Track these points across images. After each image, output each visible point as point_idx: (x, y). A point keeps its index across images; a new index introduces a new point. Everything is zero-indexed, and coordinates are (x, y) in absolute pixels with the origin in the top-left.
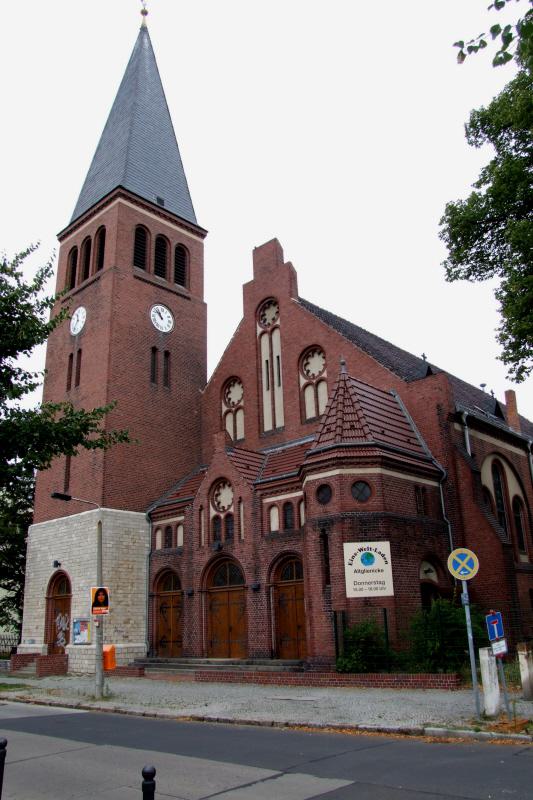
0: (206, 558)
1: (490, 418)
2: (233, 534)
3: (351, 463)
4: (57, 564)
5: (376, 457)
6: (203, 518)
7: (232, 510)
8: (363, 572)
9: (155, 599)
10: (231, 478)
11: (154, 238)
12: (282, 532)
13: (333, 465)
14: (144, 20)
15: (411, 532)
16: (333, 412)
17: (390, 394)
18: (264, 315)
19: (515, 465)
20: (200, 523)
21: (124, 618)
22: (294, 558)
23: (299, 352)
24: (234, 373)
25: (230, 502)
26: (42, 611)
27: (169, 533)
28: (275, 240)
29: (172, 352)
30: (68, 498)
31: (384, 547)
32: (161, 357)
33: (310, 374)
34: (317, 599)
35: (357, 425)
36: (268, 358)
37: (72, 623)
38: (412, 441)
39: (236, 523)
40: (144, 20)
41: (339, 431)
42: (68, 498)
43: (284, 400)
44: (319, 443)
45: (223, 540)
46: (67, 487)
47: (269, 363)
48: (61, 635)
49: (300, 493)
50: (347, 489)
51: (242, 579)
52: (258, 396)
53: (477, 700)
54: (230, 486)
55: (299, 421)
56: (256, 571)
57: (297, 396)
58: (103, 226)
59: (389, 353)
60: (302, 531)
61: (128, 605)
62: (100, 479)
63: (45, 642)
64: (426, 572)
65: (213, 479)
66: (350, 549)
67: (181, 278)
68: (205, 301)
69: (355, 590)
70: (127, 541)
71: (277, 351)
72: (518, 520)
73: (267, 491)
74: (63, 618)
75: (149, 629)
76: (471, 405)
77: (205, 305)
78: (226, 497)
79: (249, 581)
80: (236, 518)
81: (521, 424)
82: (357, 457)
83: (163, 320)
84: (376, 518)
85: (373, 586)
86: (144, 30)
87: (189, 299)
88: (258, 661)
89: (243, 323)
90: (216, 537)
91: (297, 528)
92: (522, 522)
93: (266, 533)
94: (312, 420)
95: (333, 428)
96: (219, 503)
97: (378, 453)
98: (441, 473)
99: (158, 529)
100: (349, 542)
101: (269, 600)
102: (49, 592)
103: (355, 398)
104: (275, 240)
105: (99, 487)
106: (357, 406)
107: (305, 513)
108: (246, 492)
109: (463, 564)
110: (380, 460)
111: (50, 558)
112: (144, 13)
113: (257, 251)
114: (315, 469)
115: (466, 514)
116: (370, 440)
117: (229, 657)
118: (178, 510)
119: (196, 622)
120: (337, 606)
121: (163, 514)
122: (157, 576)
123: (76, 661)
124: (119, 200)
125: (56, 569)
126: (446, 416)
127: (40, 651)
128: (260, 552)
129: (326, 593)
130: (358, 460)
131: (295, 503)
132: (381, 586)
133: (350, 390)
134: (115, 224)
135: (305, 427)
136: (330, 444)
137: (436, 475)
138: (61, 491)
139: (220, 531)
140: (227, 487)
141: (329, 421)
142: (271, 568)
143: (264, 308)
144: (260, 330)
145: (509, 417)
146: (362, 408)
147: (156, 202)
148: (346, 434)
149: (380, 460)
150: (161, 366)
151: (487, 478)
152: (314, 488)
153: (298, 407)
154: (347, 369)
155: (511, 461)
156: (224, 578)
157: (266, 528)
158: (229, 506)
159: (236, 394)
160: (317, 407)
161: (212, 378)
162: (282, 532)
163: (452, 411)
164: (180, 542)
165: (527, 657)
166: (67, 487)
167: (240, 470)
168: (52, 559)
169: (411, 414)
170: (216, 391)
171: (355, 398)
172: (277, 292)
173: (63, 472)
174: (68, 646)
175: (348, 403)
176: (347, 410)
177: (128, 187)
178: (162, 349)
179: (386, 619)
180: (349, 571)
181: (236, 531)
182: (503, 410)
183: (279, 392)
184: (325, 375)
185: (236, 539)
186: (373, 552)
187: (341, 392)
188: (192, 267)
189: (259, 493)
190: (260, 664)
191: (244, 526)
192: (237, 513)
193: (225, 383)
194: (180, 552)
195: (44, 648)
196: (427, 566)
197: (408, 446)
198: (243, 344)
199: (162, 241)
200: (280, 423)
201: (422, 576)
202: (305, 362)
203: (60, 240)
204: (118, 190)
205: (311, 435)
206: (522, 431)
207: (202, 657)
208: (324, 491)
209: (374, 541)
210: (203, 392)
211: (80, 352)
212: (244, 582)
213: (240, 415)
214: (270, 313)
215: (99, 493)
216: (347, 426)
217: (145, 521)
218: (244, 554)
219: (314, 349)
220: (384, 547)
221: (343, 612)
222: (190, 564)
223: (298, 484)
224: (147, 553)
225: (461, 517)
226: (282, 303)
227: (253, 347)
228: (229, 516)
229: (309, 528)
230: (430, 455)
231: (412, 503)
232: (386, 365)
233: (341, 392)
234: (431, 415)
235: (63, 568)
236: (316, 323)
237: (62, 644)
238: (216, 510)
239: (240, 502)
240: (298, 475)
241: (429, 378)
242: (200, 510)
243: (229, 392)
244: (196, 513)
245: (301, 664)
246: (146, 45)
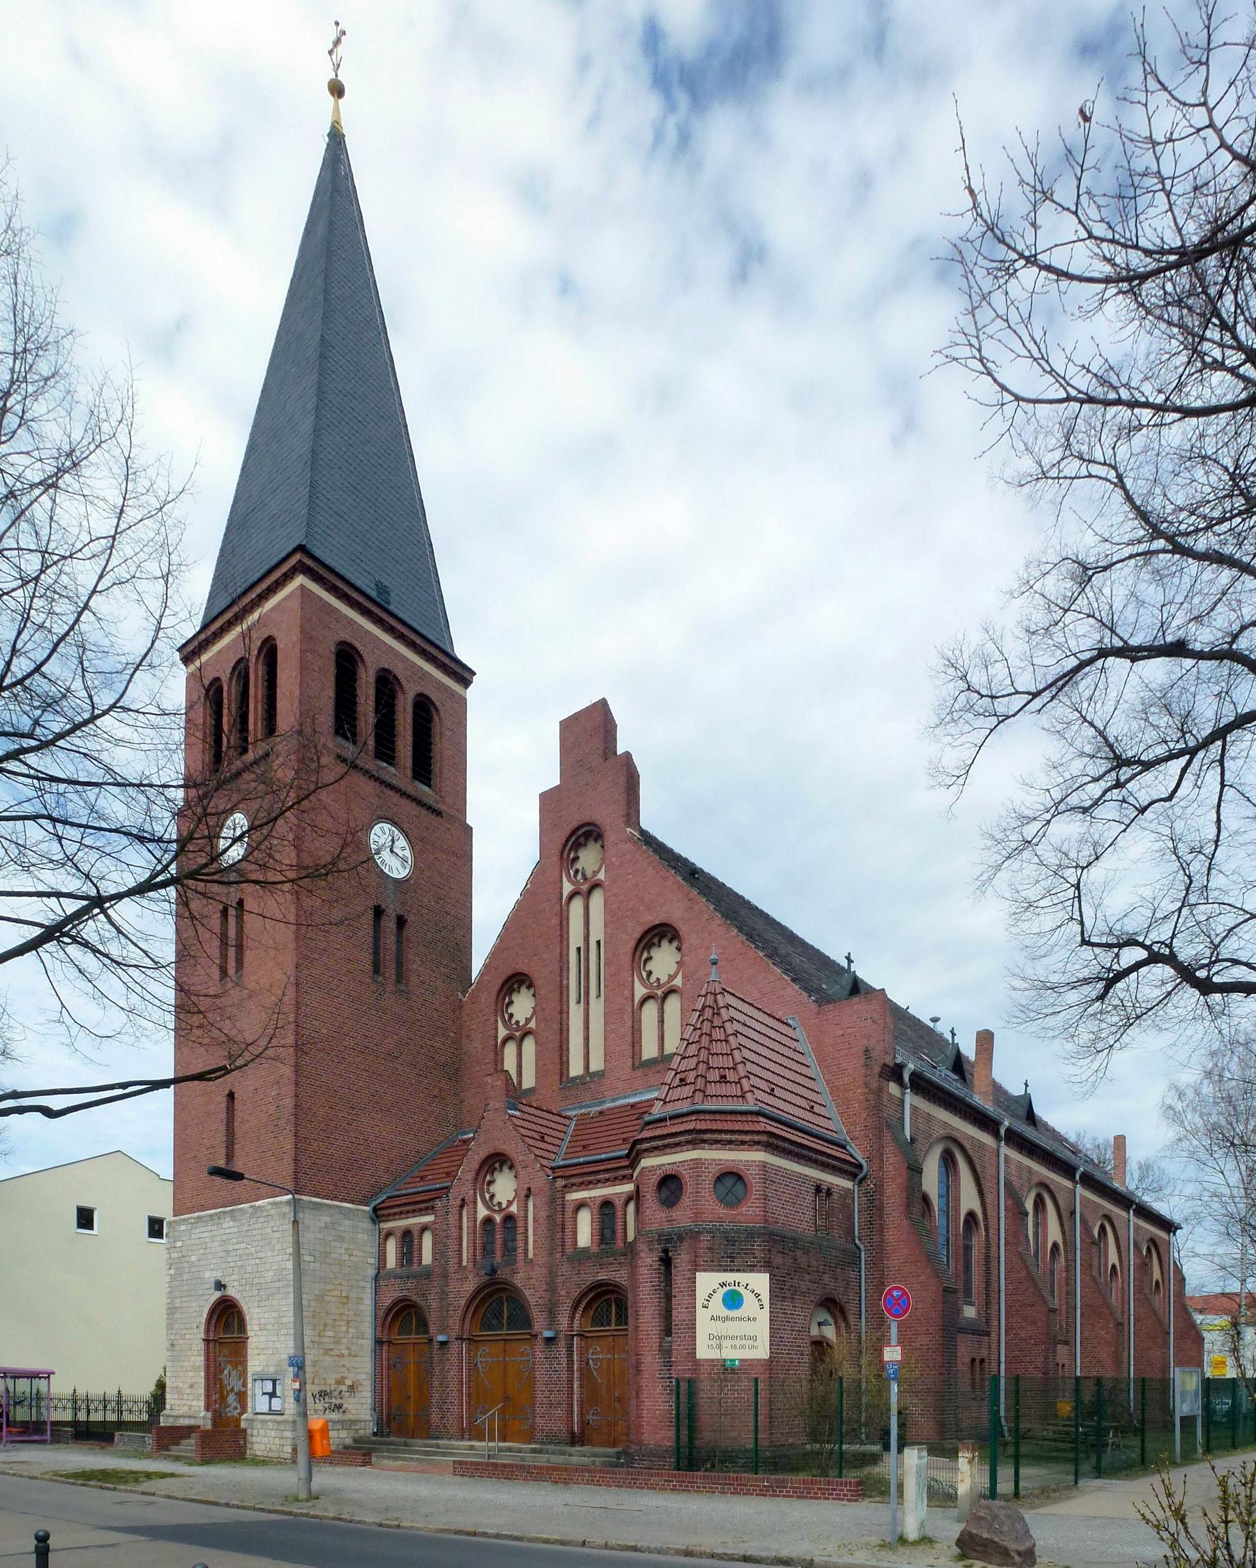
0: (470, 1286)
1: (943, 1076)
2: (515, 1249)
3: (717, 1142)
4: (220, 1286)
5: (758, 1133)
6: (465, 1220)
7: (514, 1209)
8: (727, 1319)
9: (385, 1347)
10: (513, 1155)
11: (371, 678)
12: (595, 1249)
13: (688, 1142)
14: (337, 109)
15: (803, 1261)
16: (693, 1050)
17: (790, 1026)
18: (576, 859)
19: (976, 1161)
20: (461, 1228)
22: (613, 1292)
23: (637, 935)
24: (521, 968)
25: (511, 1196)
26: (200, 1360)
27: (408, 1240)
28: (603, 703)
29: (411, 918)
30: (238, 1177)
31: (760, 1282)
32: (389, 924)
33: (653, 979)
35: (731, 1076)
36: (581, 944)
37: (250, 1380)
38: (817, 1109)
39: (520, 1230)
40: (337, 109)
41: (700, 1083)
42: (238, 1177)
43: (606, 1023)
44: (665, 1103)
45: (498, 1259)
46: (230, 1156)
47: (584, 953)
48: (231, 1399)
49: (629, 1187)
50: (707, 1184)
51: (527, 1322)
52: (561, 1013)
53: (894, 1517)
54: (511, 1168)
55: (630, 1063)
56: (552, 1314)
57: (627, 1017)
59: (790, 950)
60: (631, 1251)
61: (343, 1356)
62: (289, 1145)
63: (207, 1408)
64: (820, 1324)
65: (483, 1153)
66: (707, 1282)
67: (423, 768)
71: (597, 932)
72: (967, 1249)
73: (573, 1180)
74: (234, 1373)
75: (376, 1392)
76: (915, 1051)
77: (469, 830)
78: (504, 1187)
80: (520, 1223)
81: (995, 1095)
82: (727, 1132)
84: (751, 1234)
85: (738, 1342)
86: (336, 140)
87: (439, 813)
88: (551, 1447)
89: (539, 873)
90: (487, 1250)
91: (620, 1244)
92: (975, 1252)
93: (569, 1250)
94: (653, 1062)
95: (691, 1079)
96: (492, 1196)
97: (764, 1125)
98: (860, 1166)
99: (389, 1234)
100: (705, 1270)
101: (570, 1355)
102: (207, 1331)
103: (730, 1028)
104: (603, 703)
105: (289, 1158)
106: (733, 1041)
107: (637, 1220)
108: (539, 1180)
110: (764, 1138)
111: (207, 1275)
112: (337, 90)
114: (656, 1148)
115: (891, 1236)
116: (750, 1106)
118: (423, 1203)
119: (453, 1385)
120: (681, 1370)
121: (397, 1210)
122: (389, 1310)
123: (259, 1439)
124: (300, 580)
125: (218, 1294)
126: (877, 1070)
128: (560, 1280)
129: (666, 1352)
130: (728, 1137)
131: (619, 1204)
132: (751, 1342)
133: (723, 1011)
134: (295, 637)
135: (638, 1073)
136: (684, 1107)
137: (852, 1170)
138: (221, 1163)
139: (493, 1243)
140: (505, 1169)
141: (686, 1064)
142: (575, 1308)
143: (577, 846)
144: (568, 888)
145: (978, 1080)
146: (740, 1047)
147: (374, 594)
148: (712, 1089)
149: (764, 1138)
151: (931, 1181)
152: (654, 1180)
153: (629, 1038)
154: (719, 973)
155: (970, 1151)
156: (498, 1315)
157: (569, 1242)
158: (510, 1203)
159: (522, 1006)
160: (520, 1055)
161: (482, 974)
162: (595, 1249)
163: (889, 1060)
164: (427, 1257)
165: (970, 1462)
166: (230, 1156)
167: (531, 1142)
168: (210, 1276)
169: (821, 1061)
170: (488, 998)
171: (730, 1028)
172: (607, 816)
173: (223, 1128)
174: (244, 1416)
175: (718, 1035)
176: (716, 1048)
177: (318, 553)
178: (391, 911)
179: (757, 1393)
180: (702, 1316)
181: (520, 1244)
182: (966, 1066)
183: (597, 1008)
184: (678, 982)
185: (520, 1257)
186: (741, 1290)
187: (708, 1013)
188: (441, 747)
189: (560, 1183)
190: (553, 1453)
191: (532, 1239)
192: (522, 1213)
194: (427, 1274)
196: (823, 1315)
197: (809, 1116)
199: (387, 684)
200: (597, 1064)
201: (815, 1331)
202: (645, 955)
203: (186, 660)
204: (298, 557)
205: (650, 1088)
206: (998, 1103)
207: (462, 1439)
208: (670, 1184)
212: (530, 1326)
213: (529, 1045)
214: (589, 858)
215: (287, 1169)
216: (714, 1075)
218: (533, 1281)
219: (660, 933)
220: (760, 1282)
221: (690, 1381)
222: (443, 1295)
223: (626, 1172)
224: (371, 1272)
225: (882, 1241)
226: (610, 836)
227: (555, 921)
228: (509, 1218)
229: (642, 1247)
230: (843, 1136)
231: (809, 1215)
232: (786, 971)
233: (708, 1013)
234: (853, 1067)
235: (231, 1292)
236: (669, 883)
237: (235, 1413)
238: (488, 1208)
239: (527, 1196)
240: (628, 1156)
241: (855, 999)
242: (462, 1207)
243: (511, 1003)
244: (454, 1210)
245: (618, 1455)
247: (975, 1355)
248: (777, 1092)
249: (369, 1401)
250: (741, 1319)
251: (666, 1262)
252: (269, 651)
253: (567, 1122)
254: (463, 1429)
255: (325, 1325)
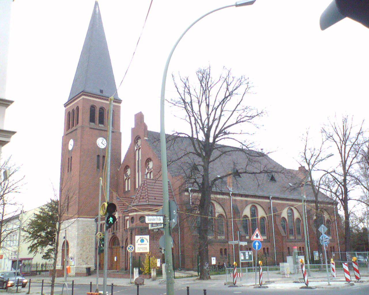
8: (141, 245)
21: (86, 257)
28: (141, 112)
31: (148, 237)
32: (101, 158)
34: (230, 237)
47: (138, 161)
51: (119, 244)
58: (78, 106)
66: (137, 238)
68: (121, 131)
69: (138, 250)
70: (87, 229)
79: (121, 245)
83: (101, 143)
85: (143, 249)
100: (137, 235)
104: (141, 112)
109: (131, 248)
113: (135, 115)
117: (248, 262)
127: (60, 269)
128: (124, 235)
144: (136, 148)
150: (101, 162)
186: (144, 239)
193: (125, 167)
195: (61, 267)
198: (131, 152)
203: (65, 106)
209: (144, 235)
210: (119, 170)
211: (71, 157)
212: (119, 245)
216: (142, 197)
217: (94, 222)
220: (148, 237)
227: (133, 155)
246: (97, 11)
247: (264, 247)
248: (157, 198)
249: (94, 262)
250: (144, 244)
251: (131, 233)
252: (78, 108)
253: (132, 199)
254: (109, 267)
255: (84, 246)
